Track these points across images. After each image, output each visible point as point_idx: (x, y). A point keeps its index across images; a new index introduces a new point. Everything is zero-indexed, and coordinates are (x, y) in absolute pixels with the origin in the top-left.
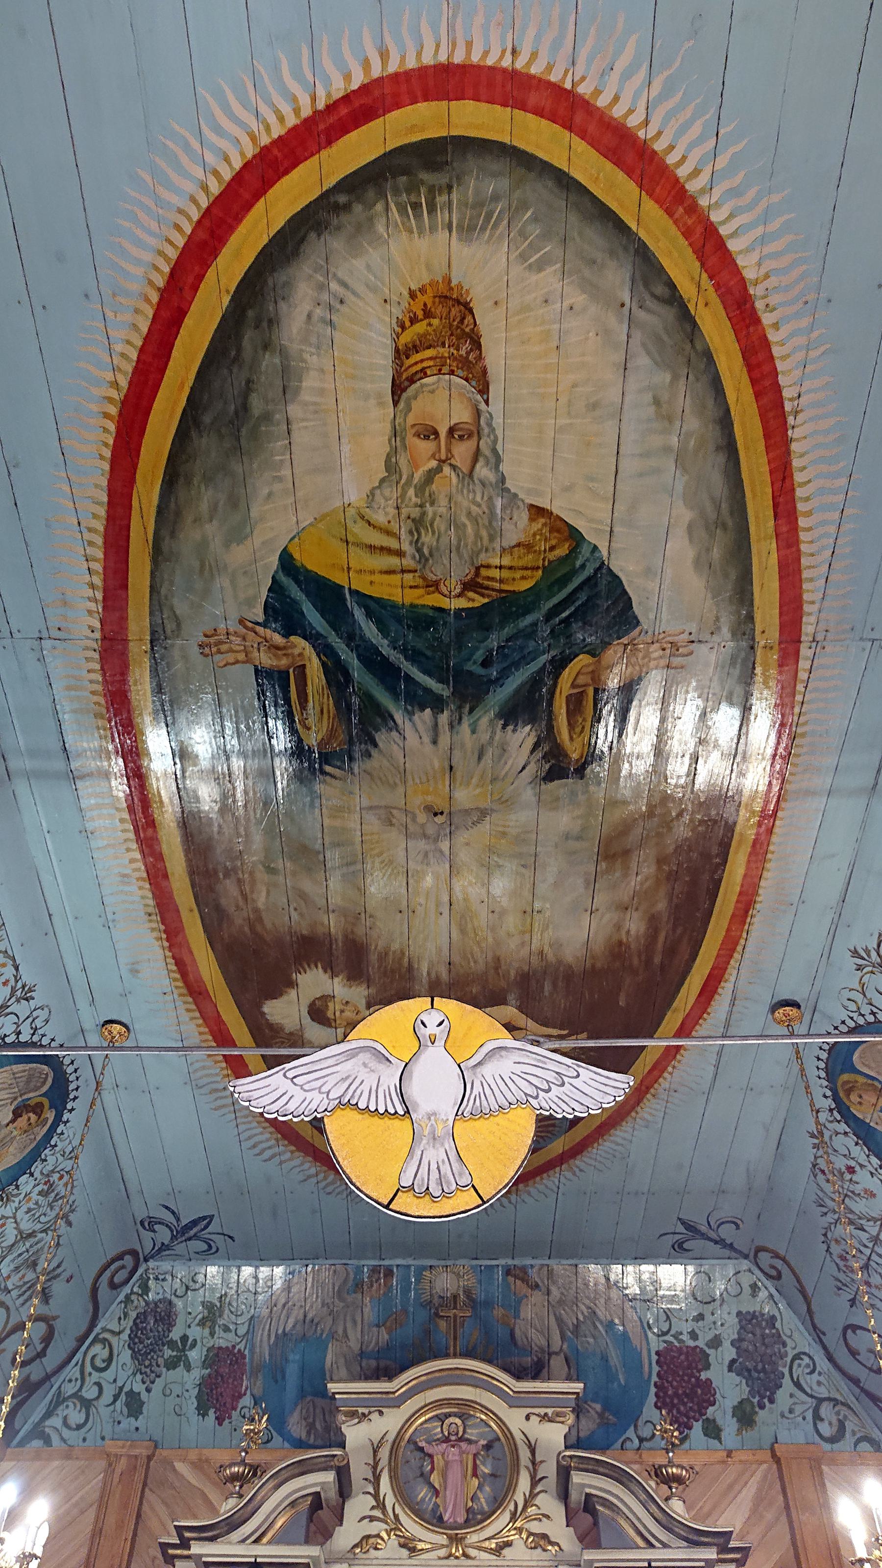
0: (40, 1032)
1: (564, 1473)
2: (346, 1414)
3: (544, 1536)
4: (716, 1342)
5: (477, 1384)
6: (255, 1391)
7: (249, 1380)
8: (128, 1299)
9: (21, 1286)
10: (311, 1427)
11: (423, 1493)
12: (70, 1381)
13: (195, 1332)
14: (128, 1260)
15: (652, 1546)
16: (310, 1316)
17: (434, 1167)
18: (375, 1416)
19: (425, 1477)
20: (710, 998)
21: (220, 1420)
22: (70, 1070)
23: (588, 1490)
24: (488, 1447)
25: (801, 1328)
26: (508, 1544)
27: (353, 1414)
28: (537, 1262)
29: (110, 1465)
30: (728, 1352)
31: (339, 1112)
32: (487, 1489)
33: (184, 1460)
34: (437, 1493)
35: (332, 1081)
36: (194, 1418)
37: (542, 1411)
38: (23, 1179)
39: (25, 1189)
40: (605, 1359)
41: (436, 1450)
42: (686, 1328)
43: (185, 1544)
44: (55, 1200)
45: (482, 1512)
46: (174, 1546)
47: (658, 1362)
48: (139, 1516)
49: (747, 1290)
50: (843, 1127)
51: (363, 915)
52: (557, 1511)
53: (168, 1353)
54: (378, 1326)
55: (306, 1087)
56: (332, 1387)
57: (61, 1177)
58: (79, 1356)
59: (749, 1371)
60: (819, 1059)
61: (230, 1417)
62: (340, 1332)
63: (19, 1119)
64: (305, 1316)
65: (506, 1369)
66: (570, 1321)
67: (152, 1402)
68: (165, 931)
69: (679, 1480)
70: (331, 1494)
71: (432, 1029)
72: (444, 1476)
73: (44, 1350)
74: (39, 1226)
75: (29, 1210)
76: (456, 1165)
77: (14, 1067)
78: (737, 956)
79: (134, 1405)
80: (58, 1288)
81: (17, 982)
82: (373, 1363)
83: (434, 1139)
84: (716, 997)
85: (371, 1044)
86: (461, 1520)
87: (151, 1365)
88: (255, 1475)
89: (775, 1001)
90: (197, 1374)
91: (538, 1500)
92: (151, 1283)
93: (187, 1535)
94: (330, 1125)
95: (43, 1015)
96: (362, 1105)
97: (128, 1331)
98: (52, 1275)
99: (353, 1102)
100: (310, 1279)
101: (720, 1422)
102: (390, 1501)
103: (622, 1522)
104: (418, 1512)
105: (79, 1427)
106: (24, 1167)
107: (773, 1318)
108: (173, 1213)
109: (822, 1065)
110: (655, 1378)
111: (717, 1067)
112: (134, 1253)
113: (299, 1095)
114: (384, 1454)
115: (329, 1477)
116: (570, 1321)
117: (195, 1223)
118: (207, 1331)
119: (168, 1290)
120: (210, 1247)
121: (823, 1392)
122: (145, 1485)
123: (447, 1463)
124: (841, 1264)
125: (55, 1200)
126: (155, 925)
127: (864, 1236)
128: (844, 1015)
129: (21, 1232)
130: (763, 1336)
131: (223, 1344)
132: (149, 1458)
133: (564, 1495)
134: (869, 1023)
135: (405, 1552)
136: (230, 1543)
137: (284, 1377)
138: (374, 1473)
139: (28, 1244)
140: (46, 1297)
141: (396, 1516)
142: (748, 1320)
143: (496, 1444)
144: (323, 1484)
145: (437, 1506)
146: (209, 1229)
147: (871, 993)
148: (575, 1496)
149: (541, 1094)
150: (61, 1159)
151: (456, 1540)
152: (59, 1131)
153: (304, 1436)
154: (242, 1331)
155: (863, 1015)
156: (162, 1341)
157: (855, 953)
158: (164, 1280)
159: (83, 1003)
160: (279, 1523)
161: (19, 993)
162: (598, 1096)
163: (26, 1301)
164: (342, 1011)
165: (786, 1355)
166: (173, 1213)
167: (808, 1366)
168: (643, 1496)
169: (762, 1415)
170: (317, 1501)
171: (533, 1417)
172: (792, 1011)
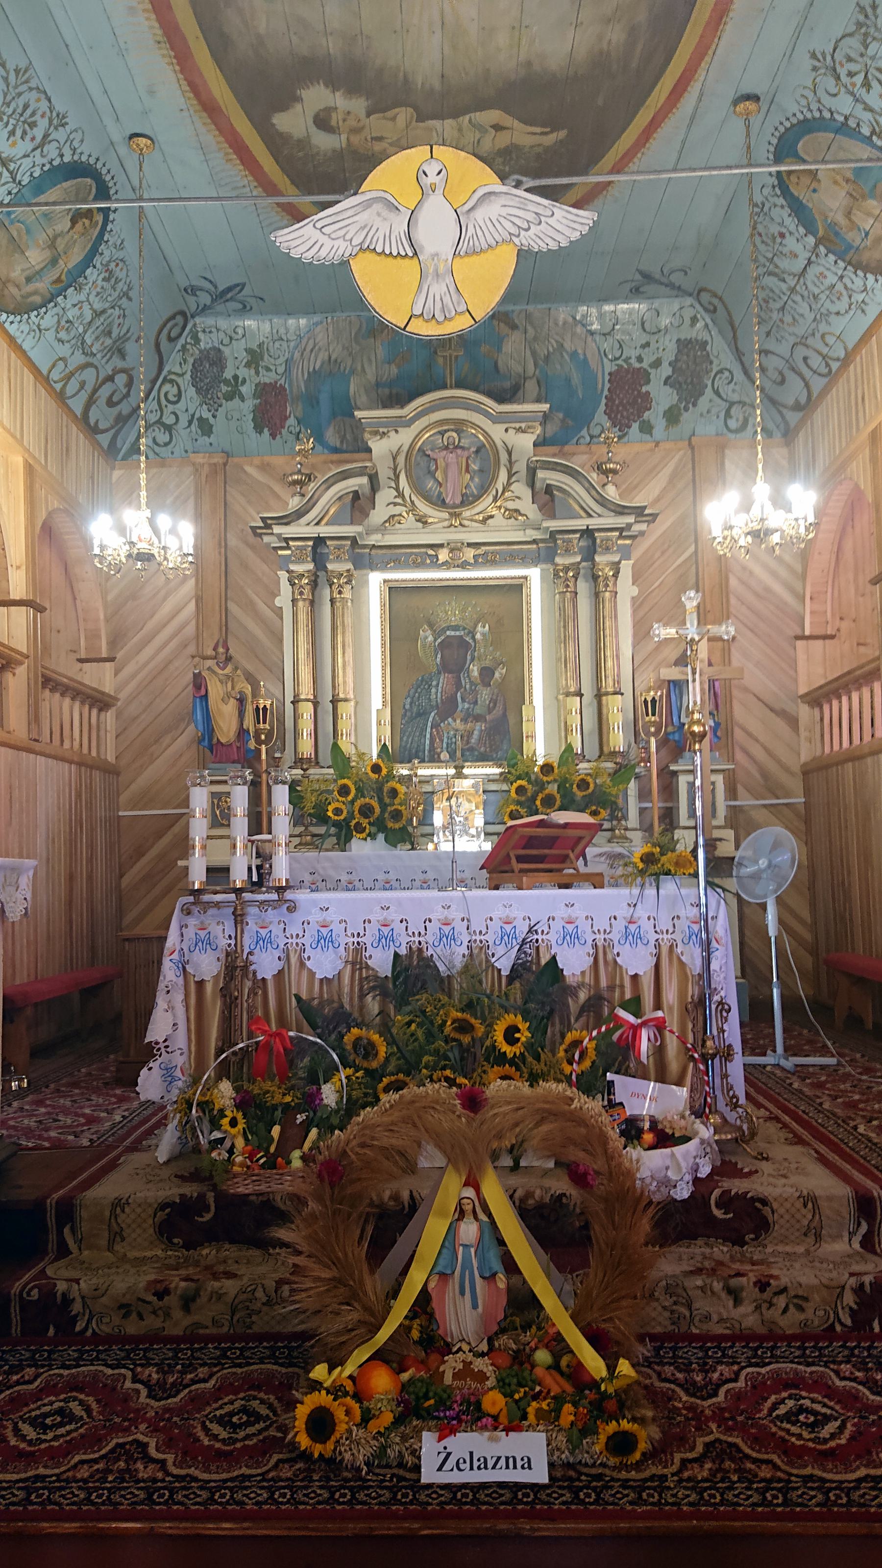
0: (79, 151)
1: (532, 472)
2: (371, 433)
3: (517, 511)
4: (657, 364)
5: (467, 408)
6: (297, 414)
7: (291, 406)
8: (184, 349)
9: (102, 351)
10: (343, 439)
11: (430, 484)
12: (152, 412)
13: (243, 372)
14: (179, 319)
15: (590, 516)
16: (333, 357)
17: (438, 298)
18: (392, 434)
19: (432, 474)
20: (678, 100)
21: (273, 436)
22: (108, 178)
23: (548, 482)
24: (477, 452)
25: (728, 350)
26: (492, 517)
27: (376, 433)
28: (517, 308)
29: (197, 470)
30: (666, 370)
31: (361, 255)
32: (476, 480)
33: (251, 465)
34: (440, 485)
35: (353, 230)
36: (253, 434)
37: (517, 425)
38: (88, 272)
39: (91, 280)
40: (568, 380)
41: (440, 456)
42: (634, 354)
43: (268, 526)
44: (116, 283)
45: (473, 495)
46: (260, 528)
47: (609, 381)
48: (225, 504)
49: (688, 321)
50: (781, 201)
51: (359, 37)
52: (527, 493)
53: (224, 388)
54: (389, 363)
55: (333, 236)
56: (358, 414)
57: (117, 265)
58: (154, 393)
59: (680, 384)
60: (776, 129)
61: (280, 433)
62: (359, 368)
63: (77, 226)
64: (330, 358)
65: (489, 394)
66: (542, 352)
67: (219, 424)
68: (175, 57)
69: (614, 472)
70: (367, 490)
71: (432, 178)
72: (445, 473)
73: (129, 391)
74: (107, 305)
75: (98, 294)
76: (455, 296)
77: (64, 184)
78: (707, 59)
79: (206, 428)
80: (130, 347)
81: (51, 112)
82: (387, 391)
83: (438, 275)
84: (686, 94)
85: (382, 194)
86: (458, 501)
87: (212, 398)
88: (310, 480)
89: (739, 94)
90: (250, 404)
91: (512, 488)
92: (201, 335)
93: (269, 522)
94: (355, 265)
95: (78, 136)
96: (379, 250)
97: (189, 373)
98: (124, 339)
99: (372, 247)
100: (331, 329)
101: (653, 422)
102: (407, 492)
103: (571, 501)
104: (427, 498)
105: (166, 444)
106: (88, 261)
107: (706, 343)
108: (211, 282)
109: (772, 149)
110: (606, 392)
111: (680, 153)
112: (183, 313)
113: (328, 244)
114: (401, 460)
115: (364, 480)
116: (542, 352)
117: (229, 289)
118: (253, 371)
119: (215, 339)
120: (245, 307)
121: (735, 397)
122: (225, 483)
123: (447, 465)
124: (764, 305)
125: (116, 283)
126: (165, 52)
127: (784, 286)
128: (795, 108)
129: (95, 311)
130: (695, 357)
131: (267, 381)
132: (225, 464)
133: (531, 483)
134: (814, 118)
135: (420, 525)
136: (299, 525)
137: (318, 402)
138: (395, 474)
139: (102, 319)
140: (122, 355)
141: (412, 502)
142: (684, 345)
143: (483, 450)
144: (360, 486)
145: (440, 493)
146: (244, 293)
147: (821, 93)
148: (538, 485)
149: (523, 233)
150: (114, 251)
151: (457, 515)
152: (108, 229)
153: (338, 445)
154: (281, 370)
155: (811, 111)
156: (218, 379)
157: (814, 56)
158: (210, 332)
159: (109, 121)
160: (332, 512)
161: (55, 122)
162: (568, 232)
163: (108, 361)
164: (344, 120)
165: (711, 370)
166: (211, 282)
167: (727, 378)
168: (587, 485)
169: (685, 416)
170: (356, 495)
171: (510, 431)
172: (750, 105)
